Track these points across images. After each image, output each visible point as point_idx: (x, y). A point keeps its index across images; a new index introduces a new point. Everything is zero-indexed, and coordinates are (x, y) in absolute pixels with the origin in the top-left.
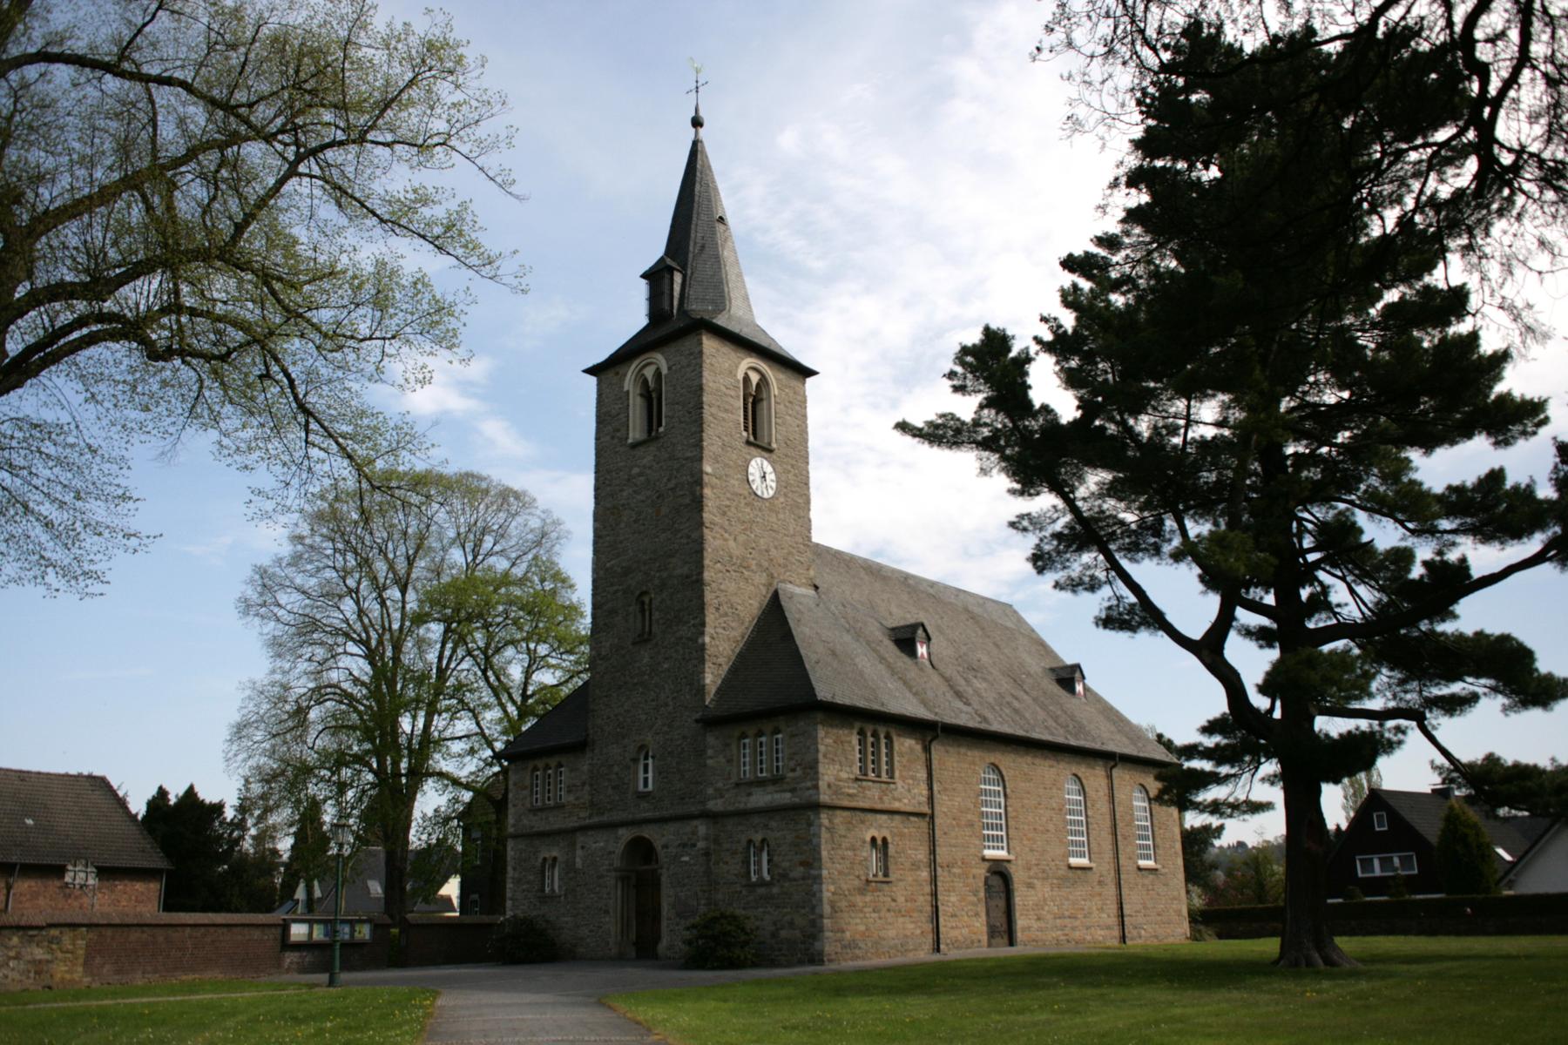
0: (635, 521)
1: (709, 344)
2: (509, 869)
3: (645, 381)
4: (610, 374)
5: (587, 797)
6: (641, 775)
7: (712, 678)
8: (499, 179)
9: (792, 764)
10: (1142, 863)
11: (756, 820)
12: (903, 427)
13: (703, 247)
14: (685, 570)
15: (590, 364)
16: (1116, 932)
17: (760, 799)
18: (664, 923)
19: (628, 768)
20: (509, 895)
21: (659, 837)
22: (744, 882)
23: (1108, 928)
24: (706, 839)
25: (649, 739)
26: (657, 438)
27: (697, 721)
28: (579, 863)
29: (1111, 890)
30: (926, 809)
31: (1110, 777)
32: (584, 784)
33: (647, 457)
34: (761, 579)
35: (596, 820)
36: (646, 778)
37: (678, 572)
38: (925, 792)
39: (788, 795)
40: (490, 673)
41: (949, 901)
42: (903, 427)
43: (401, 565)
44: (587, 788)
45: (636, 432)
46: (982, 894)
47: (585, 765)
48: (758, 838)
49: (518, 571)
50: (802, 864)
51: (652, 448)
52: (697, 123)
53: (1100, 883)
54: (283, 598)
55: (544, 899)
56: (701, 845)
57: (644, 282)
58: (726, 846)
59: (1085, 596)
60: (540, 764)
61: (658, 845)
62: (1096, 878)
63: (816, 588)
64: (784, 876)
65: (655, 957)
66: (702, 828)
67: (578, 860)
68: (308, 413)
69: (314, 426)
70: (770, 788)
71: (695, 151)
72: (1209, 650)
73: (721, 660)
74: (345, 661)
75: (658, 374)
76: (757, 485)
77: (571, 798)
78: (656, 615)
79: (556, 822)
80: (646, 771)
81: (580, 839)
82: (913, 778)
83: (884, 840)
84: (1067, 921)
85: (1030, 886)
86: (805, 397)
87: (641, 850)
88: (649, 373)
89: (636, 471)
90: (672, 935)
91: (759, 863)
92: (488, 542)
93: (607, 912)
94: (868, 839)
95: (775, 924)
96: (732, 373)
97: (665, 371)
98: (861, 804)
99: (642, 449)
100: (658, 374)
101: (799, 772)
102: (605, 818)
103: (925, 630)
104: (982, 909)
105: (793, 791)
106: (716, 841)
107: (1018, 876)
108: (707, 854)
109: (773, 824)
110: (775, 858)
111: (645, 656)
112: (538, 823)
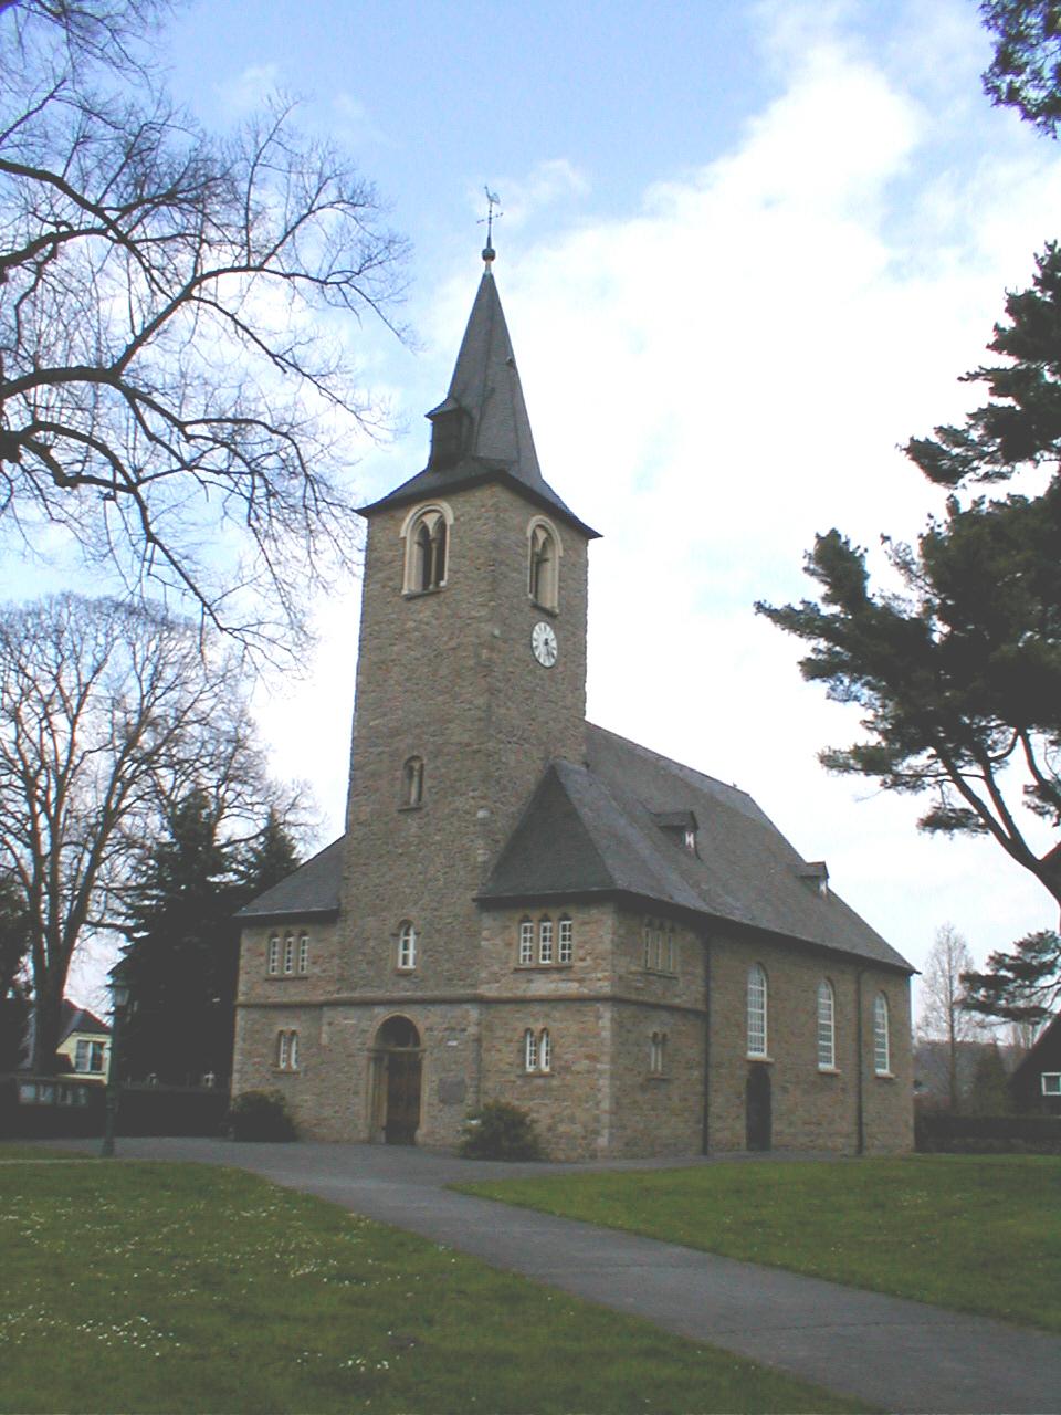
0: (407, 680)
2: (237, 1039)
3: (425, 530)
6: (401, 952)
8: (403, 335)
9: (581, 953)
11: (536, 1008)
12: (760, 607)
16: (854, 1141)
17: (542, 987)
18: (424, 1110)
19: (387, 942)
20: (236, 1066)
21: (419, 1017)
22: (519, 1072)
23: (847, 1136)
24: (478, 1024)
25: (413, 913)
26: (437, 592)
27: (474, 900)
28: (325, 1039)
29: (851, 1100)
30: (700, 1006)
31: (858, 982)
32: (333, 956)
33: (425, 611)
35: (344, 995)
36: (409, 954)
37: (455, 739)
39: (576, 985)
41: (718, 1102)
42: (760, 607)
44: (336, 961)
45: (411, 584)
47: (334, 937)
48: (538, 1026)
50: (588, 1057)
51: (432, 602)
53: (843, 1090)
55: (280, 1075)
56: (472, 1030)
57: (429, 421)
58: (500, 1033)
61: (421, 1026)
64: (567, 1069)
65: (412, 1142)
66: (474, 1013)
67: (324, 1035)
70: (555, 976)
71: (488, 289)
73: (499, 836)
75: (441, 525)
76: (541, 652)
77: (317, 970)
78: (427, 783)
79: (295, 994)
80: (406, 948)
81: (328, 1013)
83: (665, 1035)
84: (813, 1127)
85: (785, 1090)
86: (587, 561)
87: (399, 1032)
88: (431, 520)
89: (411, 624)
90: (438, 1122)
91: (536, 1053)
93: (356, 1093)
95: (553, 1116)
96: (523, 530)
97: (450, 521)
99: (420, 602)
100: (441, 525)
101: (589, 961)
102: (356, 995)
104: (743, 1112)
105: (581, 981)
106: (490, 1028)
108: (478, 1040)
109: (557, 1014)
110: (557, 1049)
111: (412, 825)
112: (276, 995)
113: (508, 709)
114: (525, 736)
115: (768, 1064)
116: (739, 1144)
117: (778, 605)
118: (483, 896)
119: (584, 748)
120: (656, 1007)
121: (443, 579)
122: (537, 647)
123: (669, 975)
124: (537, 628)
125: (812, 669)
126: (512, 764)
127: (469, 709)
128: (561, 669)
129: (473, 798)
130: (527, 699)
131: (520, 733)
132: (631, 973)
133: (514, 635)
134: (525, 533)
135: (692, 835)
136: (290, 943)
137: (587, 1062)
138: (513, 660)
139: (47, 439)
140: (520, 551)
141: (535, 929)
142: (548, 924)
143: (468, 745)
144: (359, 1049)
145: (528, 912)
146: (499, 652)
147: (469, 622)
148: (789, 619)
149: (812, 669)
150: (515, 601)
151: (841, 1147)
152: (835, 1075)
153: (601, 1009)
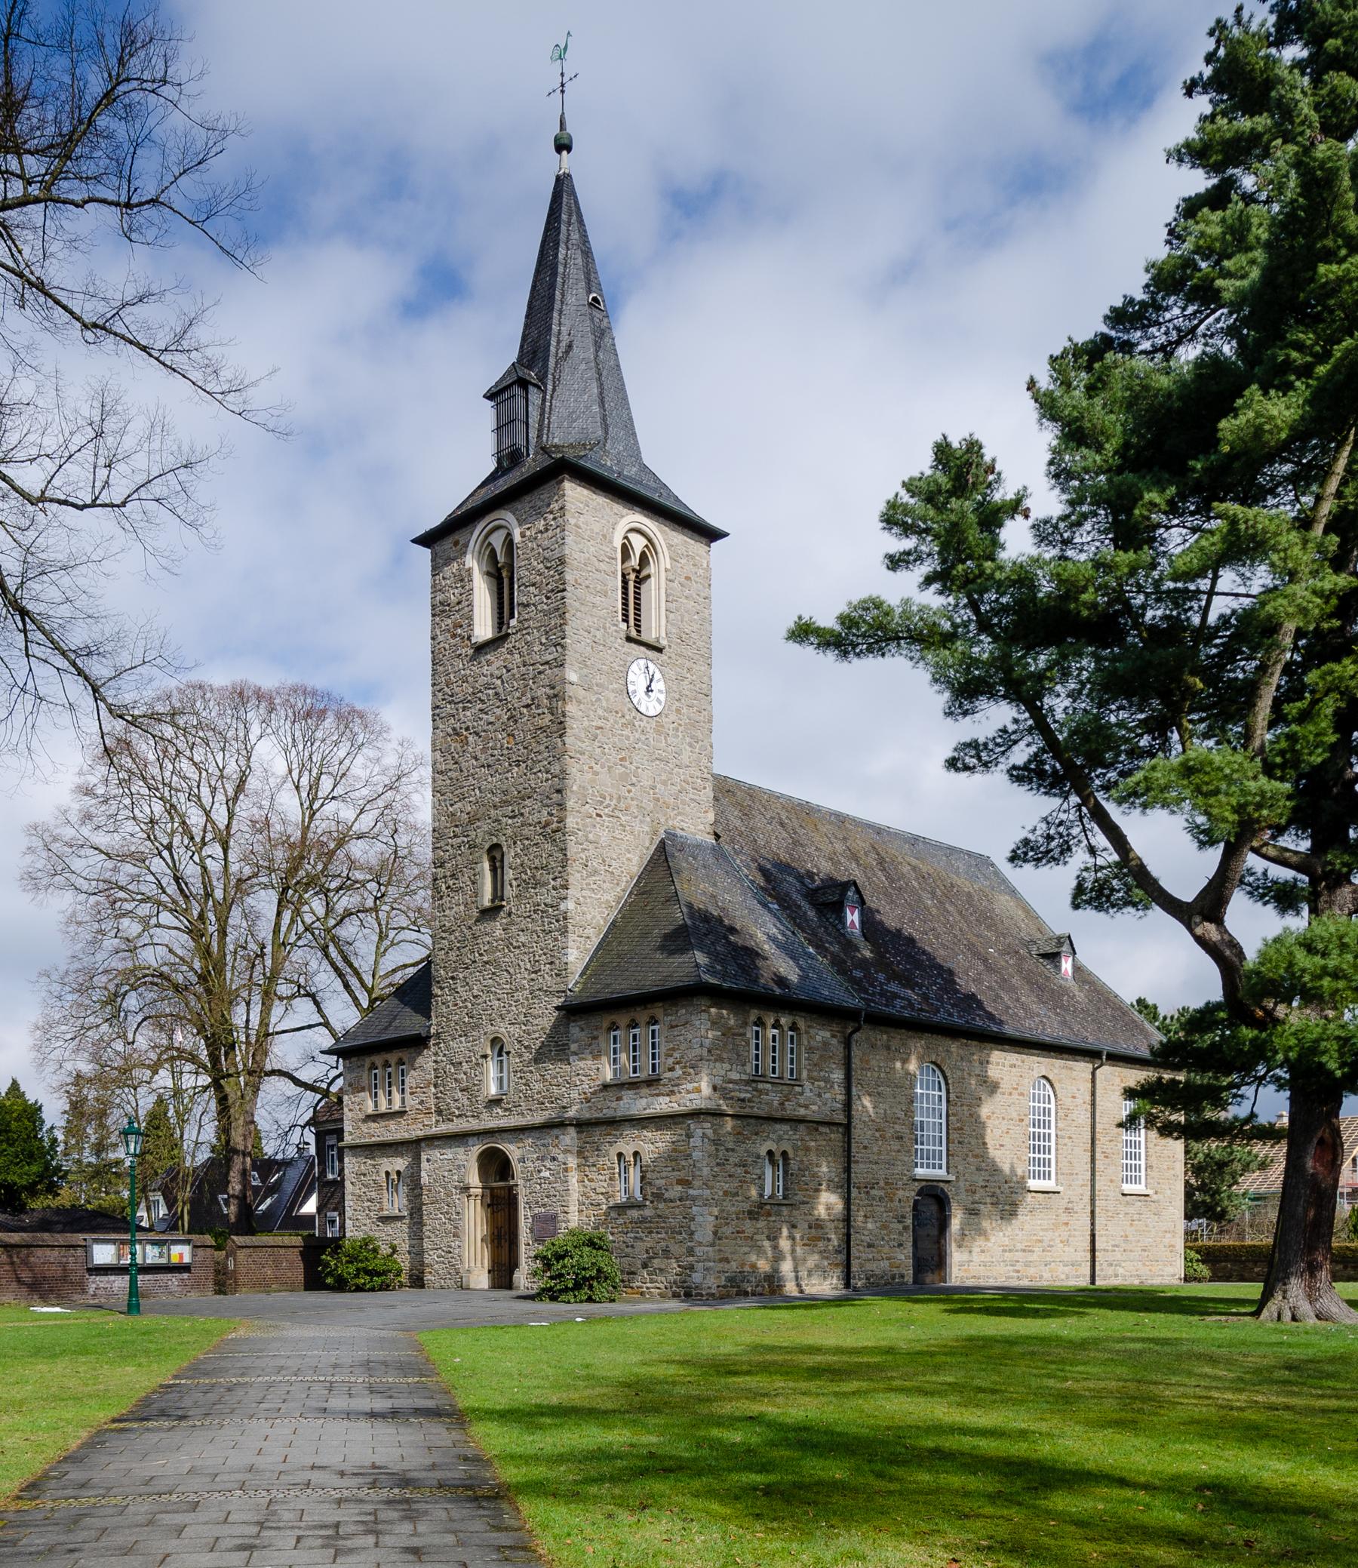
1: (574, 493)
4: (447, 544)
5: (433, 1101)
7: (577, 955)
10: (1128, 1188)
13: (570, 346)
14: (544, 816)
15: (420, 532)
21: (513, 1151)
27: (557, 1008)
30: (840, 1118)
33: (495, 661)
38: (841, 1097)
40: (332, 949)
43: (220, 816)
45: (483, 628)
46: (909, 1222)
49: (366, 822)
50: (680, 1182)
52: (563, 146)
54: (77, 864)
60: (378, 1060)
62: (1064, 1203)
63: (717, 836)
64: (658, 1196)
68: (24, 613)
69: (30, 626)
72: (1204, 911)
73: (590, 931)
74: (162, 936)
78: (509, 875)
82: (827, 1080)
83: (784, 1154)
88: (497, 540)
92: (326, 783)
94: (763, 1152)
96: (607, 538)
98: (756, 1111)
101: (679, 1072)
103: (858, 891)
104: (908, 1239)
113: (596, 774)
114: (622, 806)
115: (948, 1182)
120: (771, 1119)
122: (635, 692)
124: (634, 667)
127: (547, 780)
129: (555, 888)
130: (621, 759)
132: (731, 1082)
133: (598, 679)
134: (611, 542)
137: (680, 1188)
138: (600, 712)
139: (1126, 624)
140: (603, 566)
143: (547, 824)
145: (614, 1017)
146: (579, 702)
150: (599, 634)
151: (1063, 1277)
153: (692, 1126)
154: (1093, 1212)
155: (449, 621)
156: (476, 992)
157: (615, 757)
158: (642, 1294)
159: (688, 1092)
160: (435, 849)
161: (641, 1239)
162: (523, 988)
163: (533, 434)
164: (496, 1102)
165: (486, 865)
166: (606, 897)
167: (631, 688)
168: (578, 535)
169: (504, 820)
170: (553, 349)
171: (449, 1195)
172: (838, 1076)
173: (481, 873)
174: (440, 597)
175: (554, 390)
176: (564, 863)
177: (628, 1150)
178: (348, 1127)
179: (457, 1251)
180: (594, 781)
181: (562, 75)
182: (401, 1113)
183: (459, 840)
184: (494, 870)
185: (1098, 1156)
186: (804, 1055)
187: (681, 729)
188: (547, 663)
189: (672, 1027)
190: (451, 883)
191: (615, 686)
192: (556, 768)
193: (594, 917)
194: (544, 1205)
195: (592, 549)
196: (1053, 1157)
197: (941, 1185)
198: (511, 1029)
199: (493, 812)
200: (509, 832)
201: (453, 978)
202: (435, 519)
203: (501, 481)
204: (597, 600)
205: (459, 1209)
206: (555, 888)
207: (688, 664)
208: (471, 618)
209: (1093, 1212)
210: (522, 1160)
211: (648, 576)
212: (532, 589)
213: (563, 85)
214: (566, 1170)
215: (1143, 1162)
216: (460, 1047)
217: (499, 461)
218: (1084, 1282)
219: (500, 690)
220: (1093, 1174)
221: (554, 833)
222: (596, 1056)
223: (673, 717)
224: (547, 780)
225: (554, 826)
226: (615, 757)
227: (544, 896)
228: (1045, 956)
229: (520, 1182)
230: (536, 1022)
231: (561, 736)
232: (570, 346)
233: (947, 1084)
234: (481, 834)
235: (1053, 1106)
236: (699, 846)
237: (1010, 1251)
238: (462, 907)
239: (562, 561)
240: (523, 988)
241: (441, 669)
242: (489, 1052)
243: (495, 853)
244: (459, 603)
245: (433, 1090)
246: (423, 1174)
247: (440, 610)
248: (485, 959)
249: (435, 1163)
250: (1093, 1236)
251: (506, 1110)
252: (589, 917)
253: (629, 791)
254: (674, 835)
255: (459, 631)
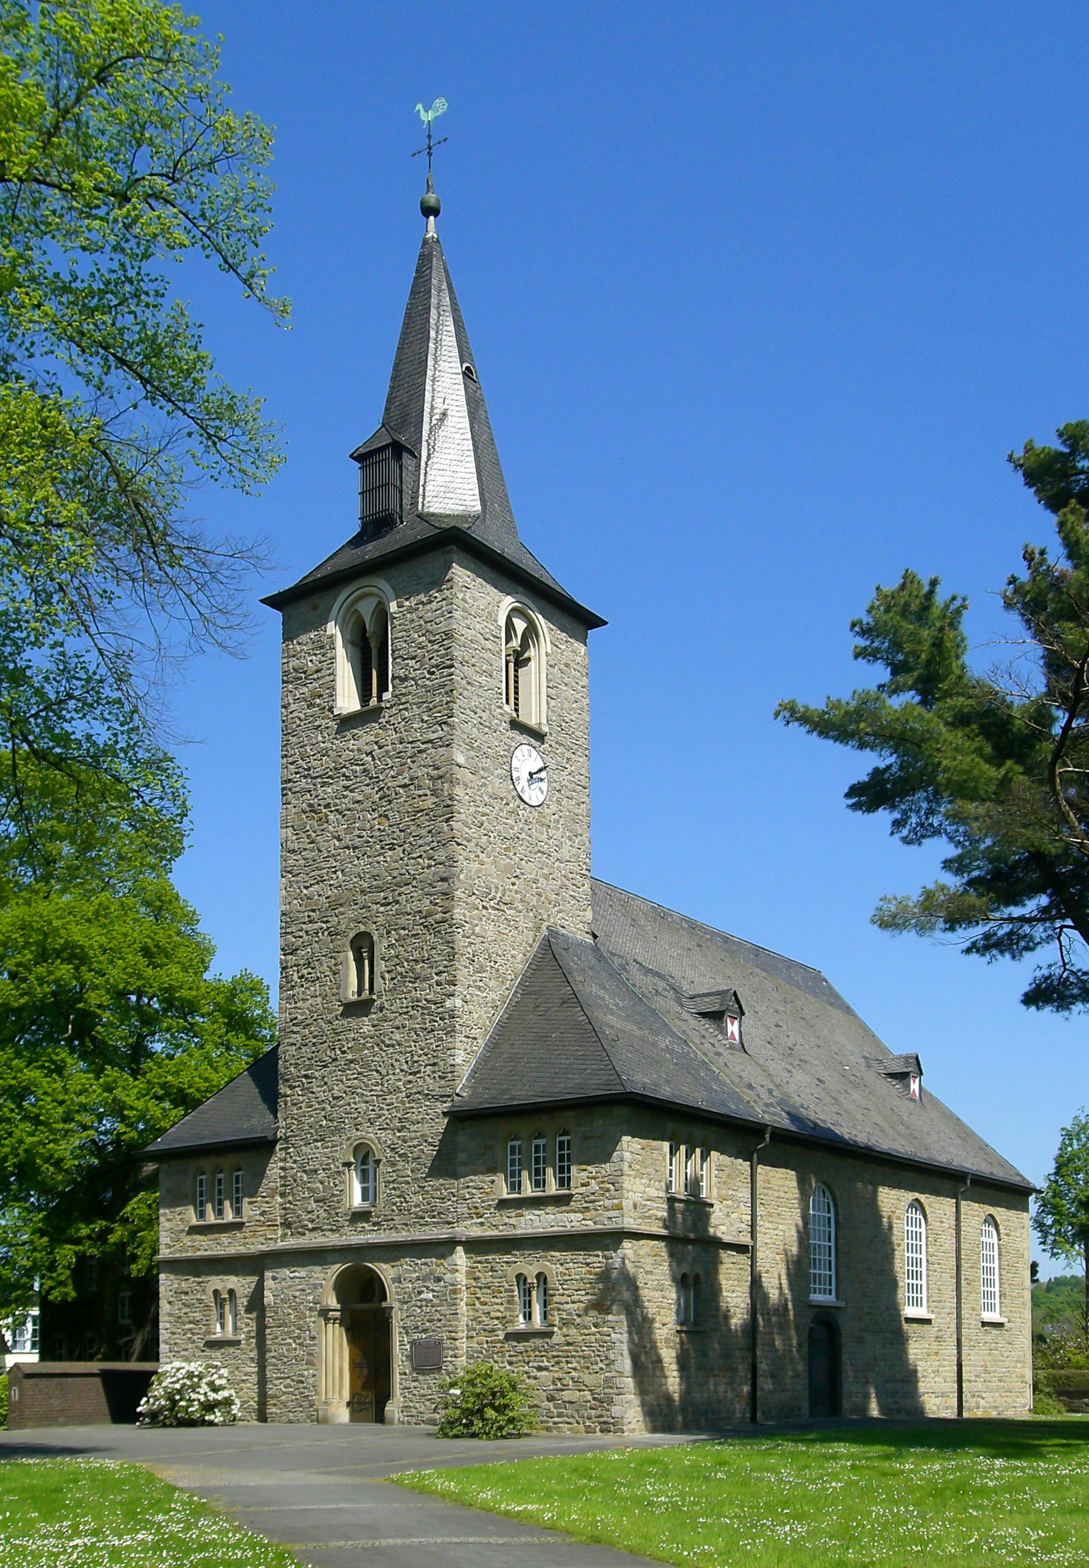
4: (303, 608)
5: (278, 1212)
7: (464, 1056)
12: (793, 714)
13: (444, 414)
21: (386, 1271)
30: (745, 1239)
33: (365, 736)
34: (525, 923)
42: (793, 714)
45: (348, 701)
59: (1005, 961)
63: (595, 937)
73: (475, 1032)
78: (381, 966)
83: (697, 1276)
85: (860, 1340)
88: (366, 609)
96: (492, 617)
107: (847, 1328)
111: (365, 1025)
114: (507, 899)
115: (838, 1308)
116: (800, 1409)
117: (817, 704)
118: (455, 1109)
119: (589, 915)
121: (387, 690)
122: (518, 779)
123: (827, 1193)
125: (870, 795)
126: (490, 935)
127: (429, 866)
128: (554, 808)
129: (438, 984)
130: (506, 849)
131: (499, 894)
135: (736, 1022)
136: (220, 1180)
141: (523, 1149)
142: (541, 1142)
143: (430, 914)
144: (310, 1309)
147: (423, 747)
148: (837, 726)
149: (870, 795)
150: (485, 716)
152: (928, 1322)
154: (959, 1341)
155: (305, 690)
156: (336, 1093)
157: (500, 846)
158: (548, 1429)
159: (606, 1209)
160: (284, 934)
161: (546, 1369)
162: (397, 1090)
163: (406, 501)
164: (360, 1216)
165: (351, 955)
166: (492, 996)
167: (515, 775)
168: (464, 610)
169: (375, 907)
170: (426, 419)
171: (302, 1317)
172: (745, 1194)
173: (344, 963)
174: (294, 663)
175: (429, 457)
176: (452, 957)
177: (531, 1272)
178: (164, 1239)
179: (311, 1380)
180: (480, 871)
181: (429, 137)
182: (239, 1226)
183: (316, 926)
184: (359, 961)
185: (963, 1283)
186: (714, 1172)
187: (562, 821)
188: (430, 741)
189: (586, 1138)
190: (305, 972)
191: (500, 771)
192: (441, 855)
193: (480, 1017)
194: (425, 1331)
195: (478, 626)
196: (924, 1282)
197: (833, 1311)
198: (382, 1135)
199: (360, 899)
200: (381, 919)
201: (306, 1076)
202: (287, 581)
203: (369, 547)
204: (483, 679)
205: (314, 1333)
206: (438, 984)
207: (568, 754)
208: (334, 688)
209: (959, 1341)
210: (398, 1280)
211: (529, 659)
212: (411, 663)
213: (430, 148)
214: (454, 1292)
215: (997, 1289)
216: (316, 1153)
217: (364, 526)
218: (950, 1414)
219: (370, 766)
220: (959, 1302)
221: (439, 924)
222: (492, 1170)
223: (554, 808)
224: (429, 866)
225: (438, 917)
226: (500, 846)
227: (425, 992)
228: (892, 1075)
229: (396, 1305)
230: (415, 1128)
231: (447, 821)
232: (444, 414)
233: (835, 1205)
234: (348, 921)
235: (923, 1230)
236: (580, 944)
237: (891, 1381)
238: (319, 999)
239: (448, 635)
240: (397, 1090)
241: (294, 740)
242: (352, 1160)
243: (363, 945)
244: (318, 671)
245: (279, 1199)
246: (267, 1293)
247: (292, 678)
248: (350, 1057)
249: (277, 1284)
250: (960, 1366)
251: (374, 1224)
252: (475, 1016)
253: (514, 884)
254: (557, 933)
255: (318, 701)
